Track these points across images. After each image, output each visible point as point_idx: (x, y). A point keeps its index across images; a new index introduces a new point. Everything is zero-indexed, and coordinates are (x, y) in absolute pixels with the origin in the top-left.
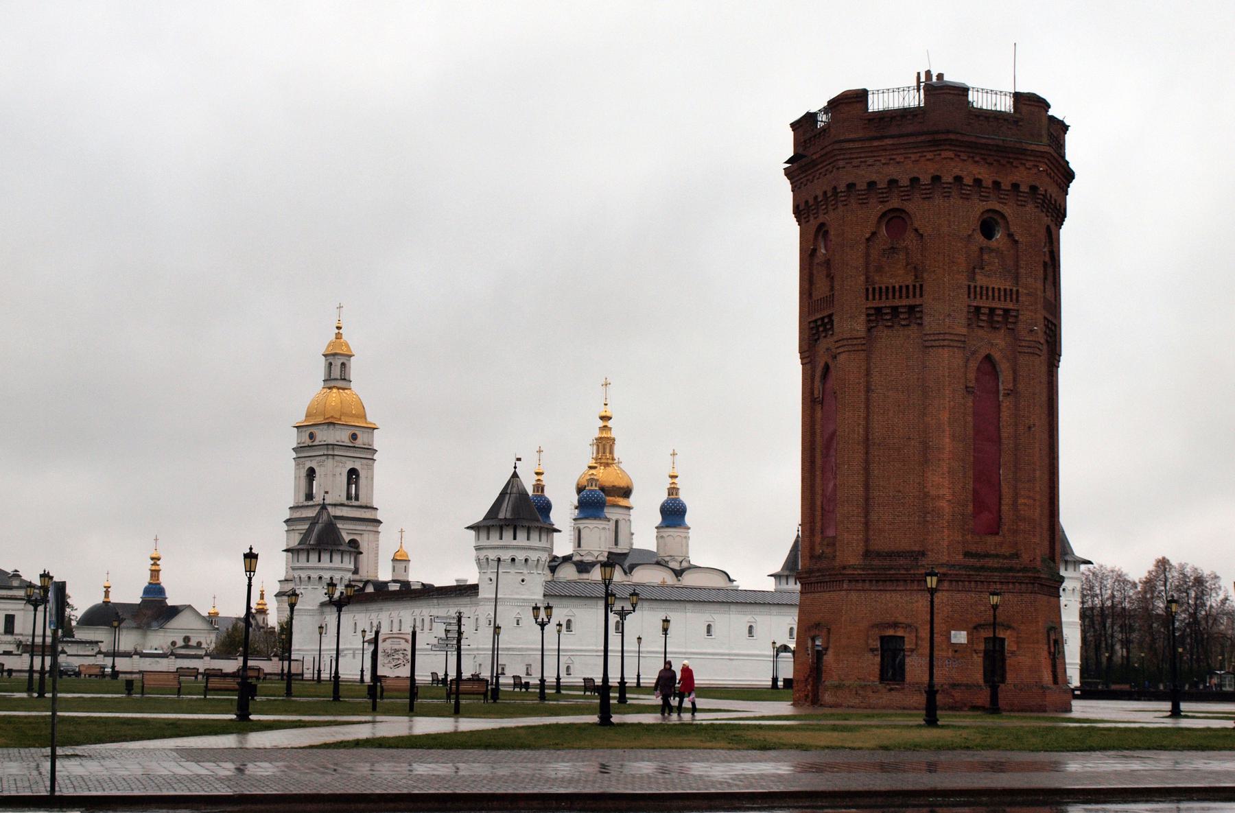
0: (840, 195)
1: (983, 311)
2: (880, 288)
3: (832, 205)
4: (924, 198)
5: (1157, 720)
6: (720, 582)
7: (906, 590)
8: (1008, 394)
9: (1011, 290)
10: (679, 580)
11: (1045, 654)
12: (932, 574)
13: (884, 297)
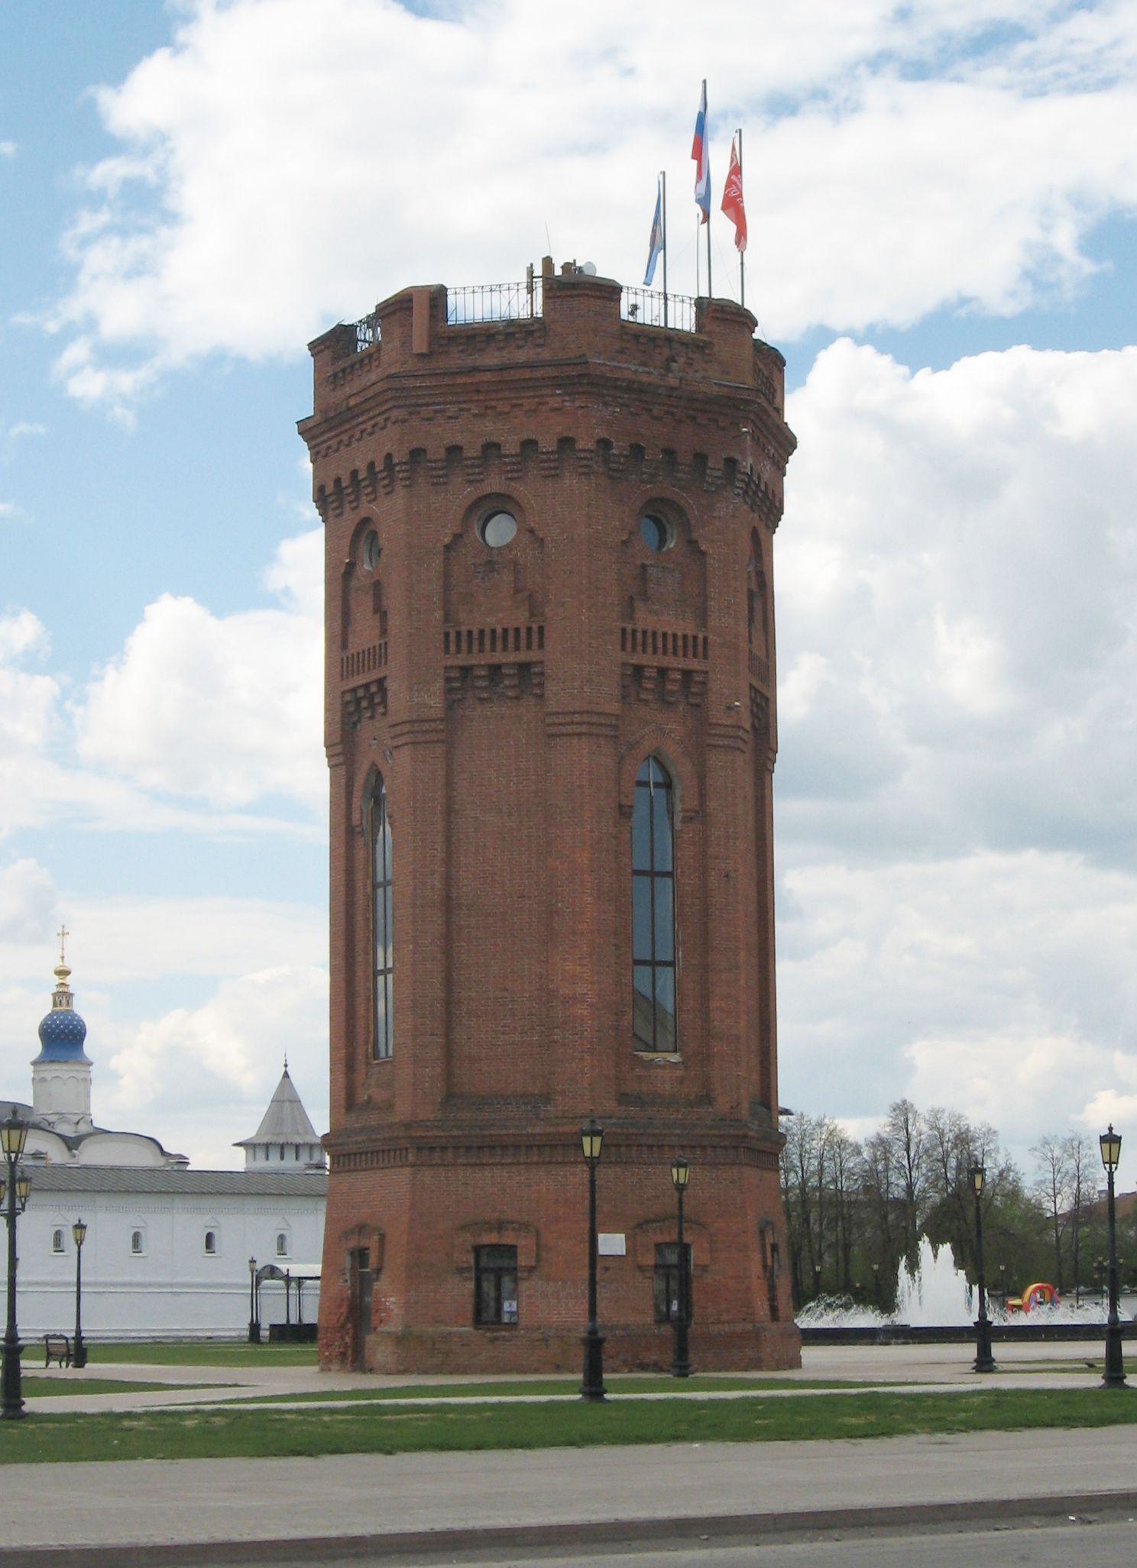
0: (397, 469)
1: (647, 673)
2: (470, 633)
3: (385, 486)
4: (546, 477)
5: (958, 1378)
6: (147, 1159)
7: (519, 1164)
8: (691, 819)
9: (695, 638)
10: (74, 1156)
11: (755, 1268)
12: (593, 1133)
13: (475, 648)
